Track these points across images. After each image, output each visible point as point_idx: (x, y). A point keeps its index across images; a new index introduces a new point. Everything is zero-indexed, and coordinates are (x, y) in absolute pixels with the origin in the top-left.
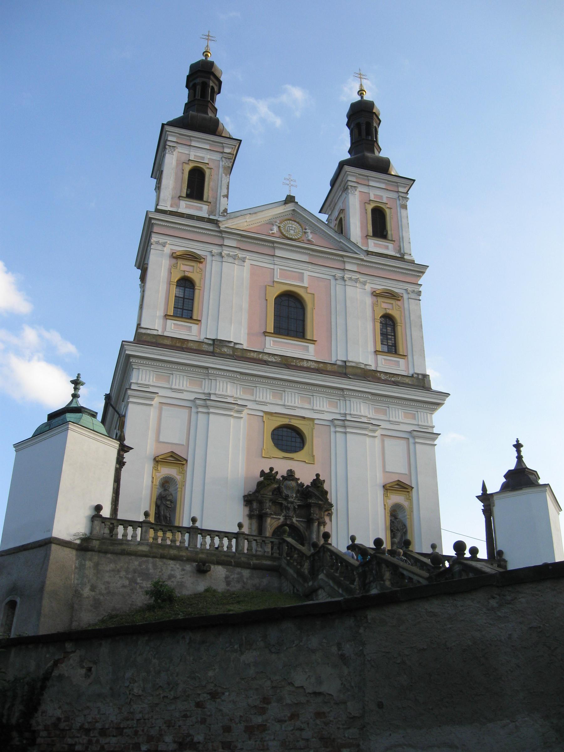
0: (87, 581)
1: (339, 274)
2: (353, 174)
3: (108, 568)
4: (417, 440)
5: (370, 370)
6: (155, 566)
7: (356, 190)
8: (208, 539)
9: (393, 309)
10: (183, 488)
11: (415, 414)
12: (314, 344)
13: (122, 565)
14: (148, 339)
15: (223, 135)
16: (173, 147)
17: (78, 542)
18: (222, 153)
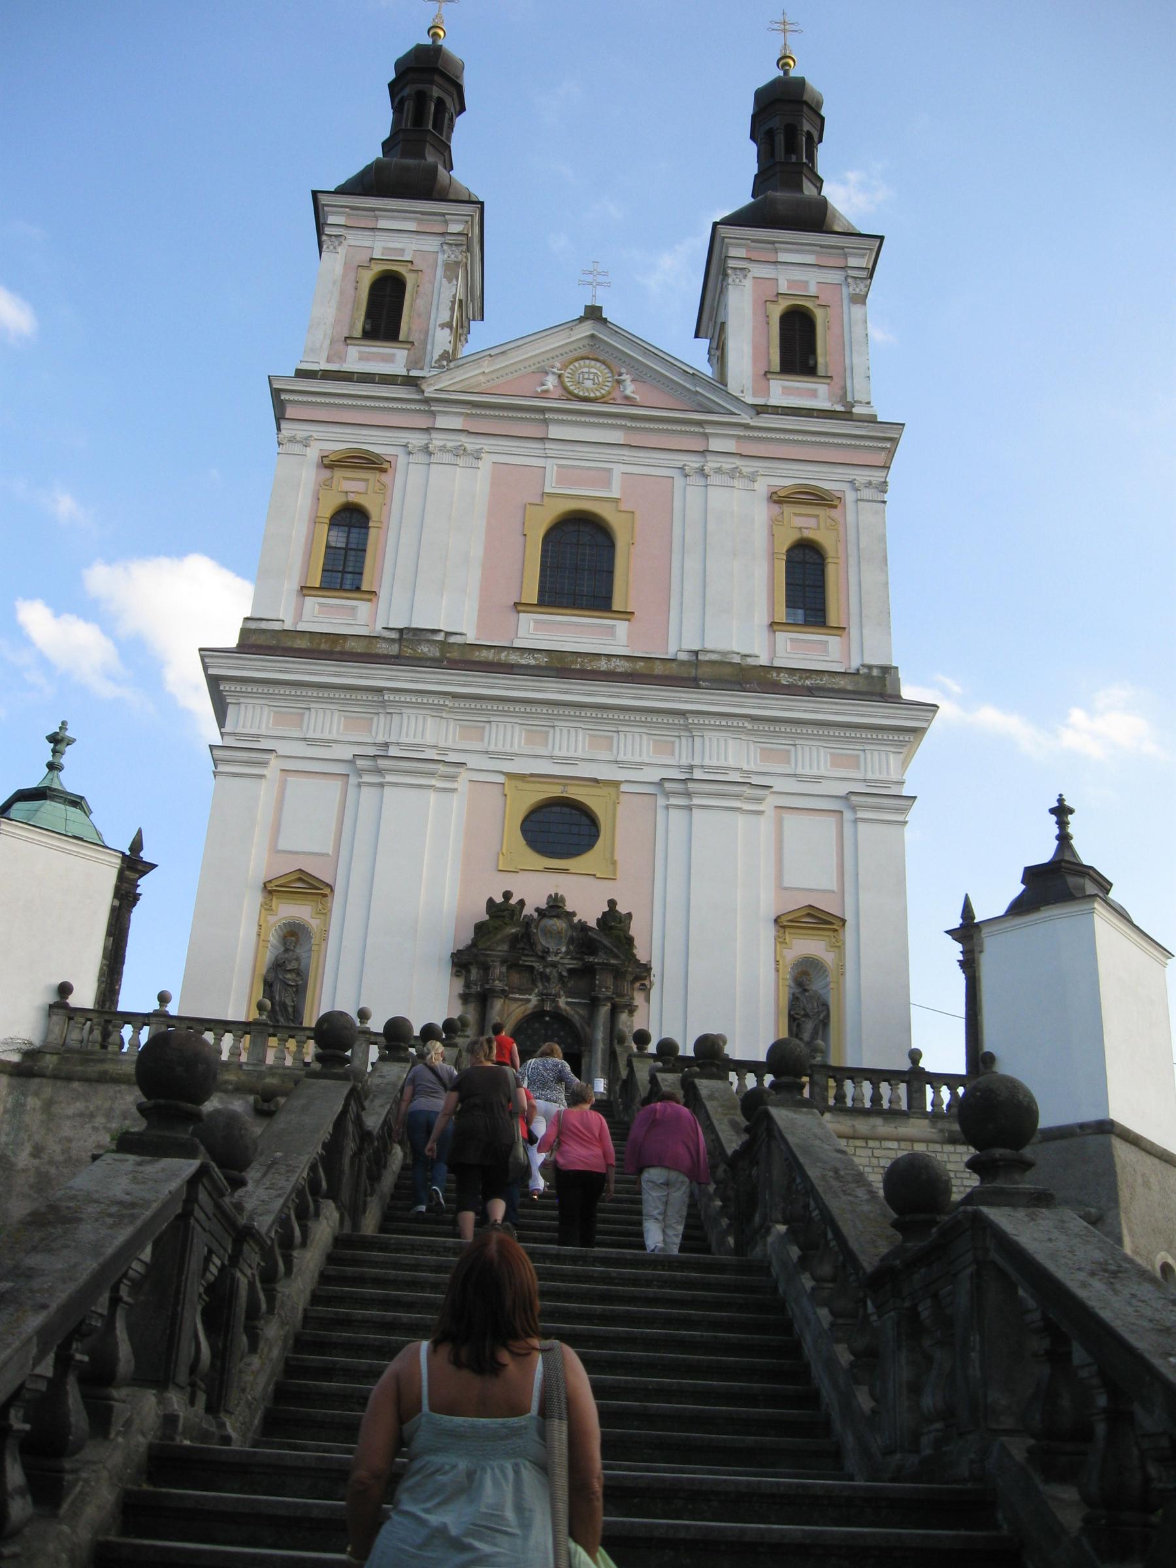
0: (26, 1138)
1: (693, 462)
3: (70, 1111)
4: (860, 815)
5: (755, 667)
7: (745, 276)
8: (867, 1087)
9: (818, 528)
10: (323, 946)
11: (789, 751)
12: (628, 620)
13: (99, 1103)
15: (452, 197)
16: (336, 236)
17: (15, 1058)
18: (443, 234)
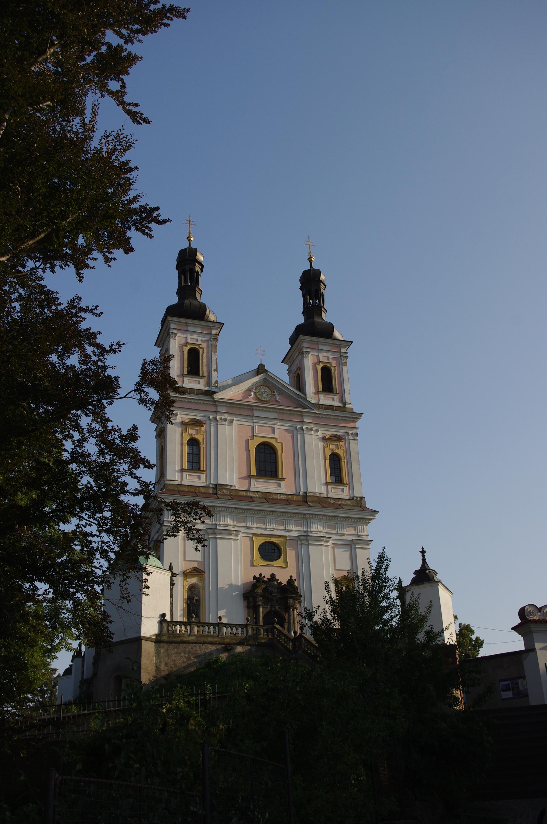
2: (305, 341)
6: (200, 648)
14: (172, 488)
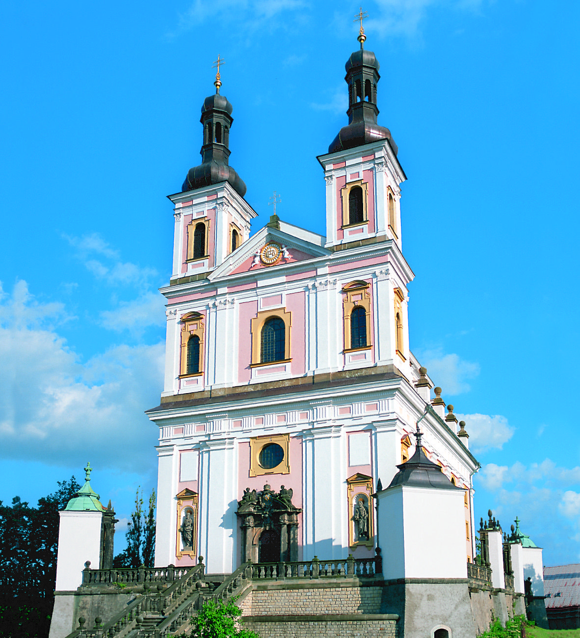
7: (332, 179)
